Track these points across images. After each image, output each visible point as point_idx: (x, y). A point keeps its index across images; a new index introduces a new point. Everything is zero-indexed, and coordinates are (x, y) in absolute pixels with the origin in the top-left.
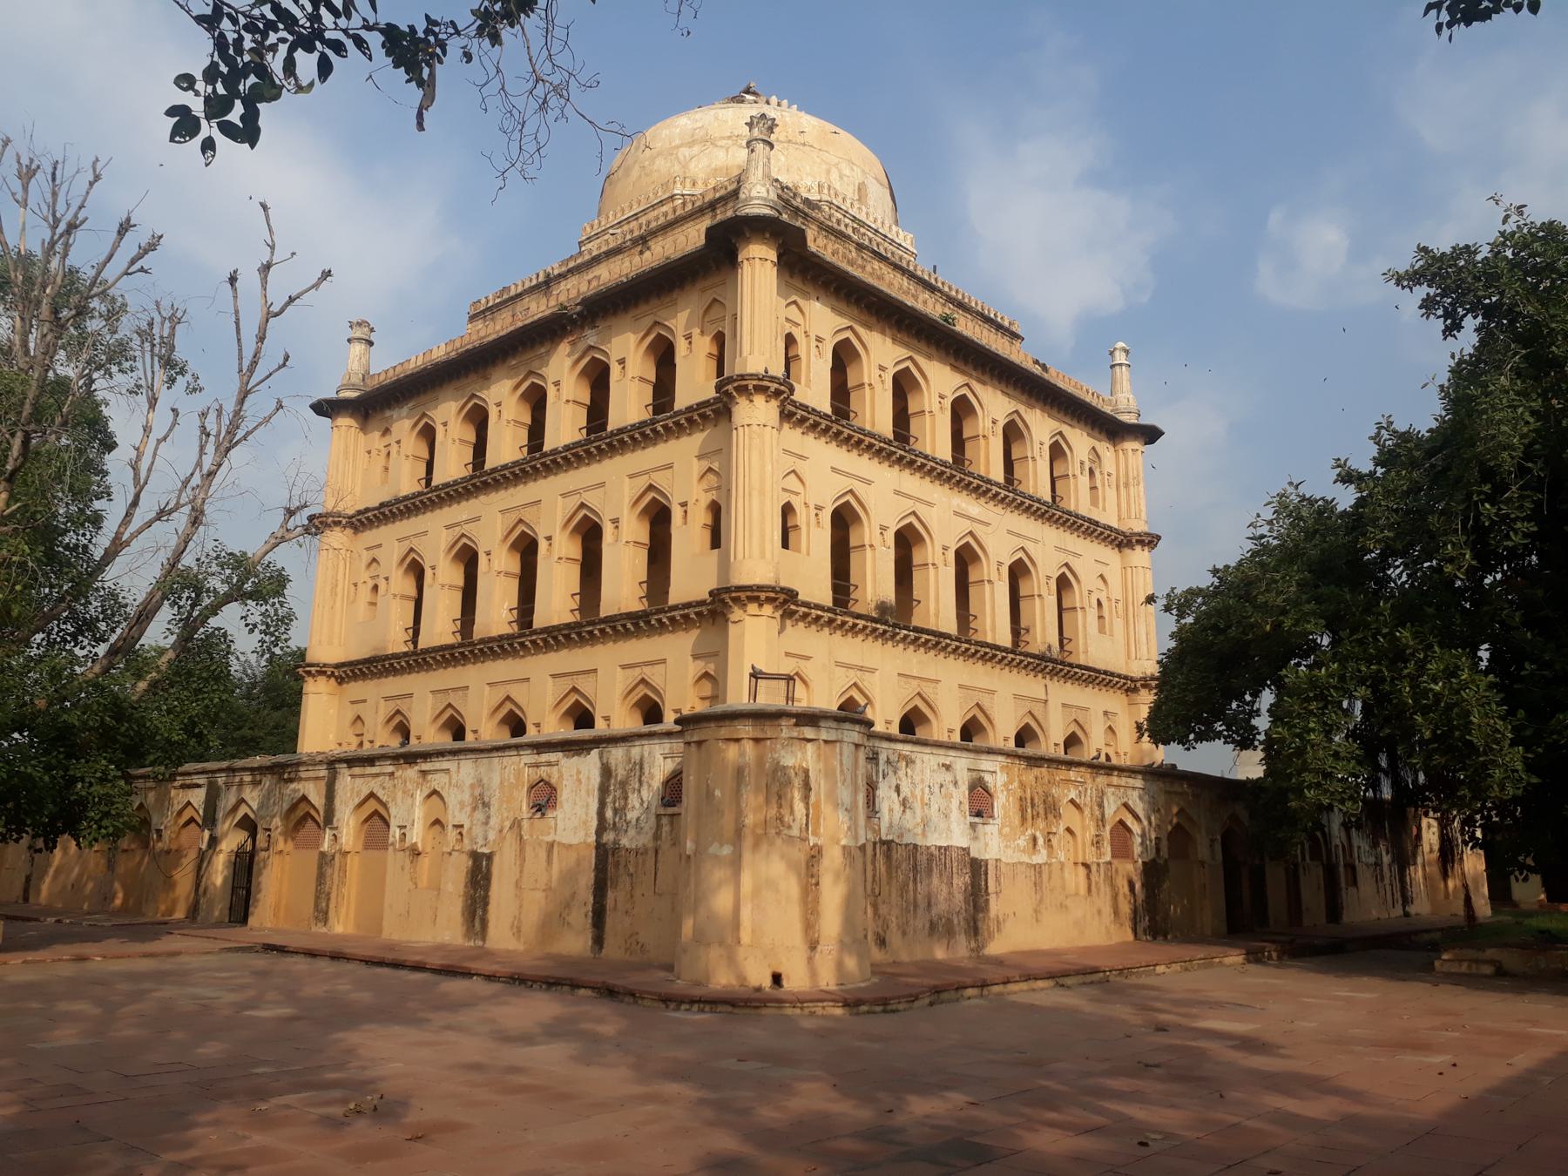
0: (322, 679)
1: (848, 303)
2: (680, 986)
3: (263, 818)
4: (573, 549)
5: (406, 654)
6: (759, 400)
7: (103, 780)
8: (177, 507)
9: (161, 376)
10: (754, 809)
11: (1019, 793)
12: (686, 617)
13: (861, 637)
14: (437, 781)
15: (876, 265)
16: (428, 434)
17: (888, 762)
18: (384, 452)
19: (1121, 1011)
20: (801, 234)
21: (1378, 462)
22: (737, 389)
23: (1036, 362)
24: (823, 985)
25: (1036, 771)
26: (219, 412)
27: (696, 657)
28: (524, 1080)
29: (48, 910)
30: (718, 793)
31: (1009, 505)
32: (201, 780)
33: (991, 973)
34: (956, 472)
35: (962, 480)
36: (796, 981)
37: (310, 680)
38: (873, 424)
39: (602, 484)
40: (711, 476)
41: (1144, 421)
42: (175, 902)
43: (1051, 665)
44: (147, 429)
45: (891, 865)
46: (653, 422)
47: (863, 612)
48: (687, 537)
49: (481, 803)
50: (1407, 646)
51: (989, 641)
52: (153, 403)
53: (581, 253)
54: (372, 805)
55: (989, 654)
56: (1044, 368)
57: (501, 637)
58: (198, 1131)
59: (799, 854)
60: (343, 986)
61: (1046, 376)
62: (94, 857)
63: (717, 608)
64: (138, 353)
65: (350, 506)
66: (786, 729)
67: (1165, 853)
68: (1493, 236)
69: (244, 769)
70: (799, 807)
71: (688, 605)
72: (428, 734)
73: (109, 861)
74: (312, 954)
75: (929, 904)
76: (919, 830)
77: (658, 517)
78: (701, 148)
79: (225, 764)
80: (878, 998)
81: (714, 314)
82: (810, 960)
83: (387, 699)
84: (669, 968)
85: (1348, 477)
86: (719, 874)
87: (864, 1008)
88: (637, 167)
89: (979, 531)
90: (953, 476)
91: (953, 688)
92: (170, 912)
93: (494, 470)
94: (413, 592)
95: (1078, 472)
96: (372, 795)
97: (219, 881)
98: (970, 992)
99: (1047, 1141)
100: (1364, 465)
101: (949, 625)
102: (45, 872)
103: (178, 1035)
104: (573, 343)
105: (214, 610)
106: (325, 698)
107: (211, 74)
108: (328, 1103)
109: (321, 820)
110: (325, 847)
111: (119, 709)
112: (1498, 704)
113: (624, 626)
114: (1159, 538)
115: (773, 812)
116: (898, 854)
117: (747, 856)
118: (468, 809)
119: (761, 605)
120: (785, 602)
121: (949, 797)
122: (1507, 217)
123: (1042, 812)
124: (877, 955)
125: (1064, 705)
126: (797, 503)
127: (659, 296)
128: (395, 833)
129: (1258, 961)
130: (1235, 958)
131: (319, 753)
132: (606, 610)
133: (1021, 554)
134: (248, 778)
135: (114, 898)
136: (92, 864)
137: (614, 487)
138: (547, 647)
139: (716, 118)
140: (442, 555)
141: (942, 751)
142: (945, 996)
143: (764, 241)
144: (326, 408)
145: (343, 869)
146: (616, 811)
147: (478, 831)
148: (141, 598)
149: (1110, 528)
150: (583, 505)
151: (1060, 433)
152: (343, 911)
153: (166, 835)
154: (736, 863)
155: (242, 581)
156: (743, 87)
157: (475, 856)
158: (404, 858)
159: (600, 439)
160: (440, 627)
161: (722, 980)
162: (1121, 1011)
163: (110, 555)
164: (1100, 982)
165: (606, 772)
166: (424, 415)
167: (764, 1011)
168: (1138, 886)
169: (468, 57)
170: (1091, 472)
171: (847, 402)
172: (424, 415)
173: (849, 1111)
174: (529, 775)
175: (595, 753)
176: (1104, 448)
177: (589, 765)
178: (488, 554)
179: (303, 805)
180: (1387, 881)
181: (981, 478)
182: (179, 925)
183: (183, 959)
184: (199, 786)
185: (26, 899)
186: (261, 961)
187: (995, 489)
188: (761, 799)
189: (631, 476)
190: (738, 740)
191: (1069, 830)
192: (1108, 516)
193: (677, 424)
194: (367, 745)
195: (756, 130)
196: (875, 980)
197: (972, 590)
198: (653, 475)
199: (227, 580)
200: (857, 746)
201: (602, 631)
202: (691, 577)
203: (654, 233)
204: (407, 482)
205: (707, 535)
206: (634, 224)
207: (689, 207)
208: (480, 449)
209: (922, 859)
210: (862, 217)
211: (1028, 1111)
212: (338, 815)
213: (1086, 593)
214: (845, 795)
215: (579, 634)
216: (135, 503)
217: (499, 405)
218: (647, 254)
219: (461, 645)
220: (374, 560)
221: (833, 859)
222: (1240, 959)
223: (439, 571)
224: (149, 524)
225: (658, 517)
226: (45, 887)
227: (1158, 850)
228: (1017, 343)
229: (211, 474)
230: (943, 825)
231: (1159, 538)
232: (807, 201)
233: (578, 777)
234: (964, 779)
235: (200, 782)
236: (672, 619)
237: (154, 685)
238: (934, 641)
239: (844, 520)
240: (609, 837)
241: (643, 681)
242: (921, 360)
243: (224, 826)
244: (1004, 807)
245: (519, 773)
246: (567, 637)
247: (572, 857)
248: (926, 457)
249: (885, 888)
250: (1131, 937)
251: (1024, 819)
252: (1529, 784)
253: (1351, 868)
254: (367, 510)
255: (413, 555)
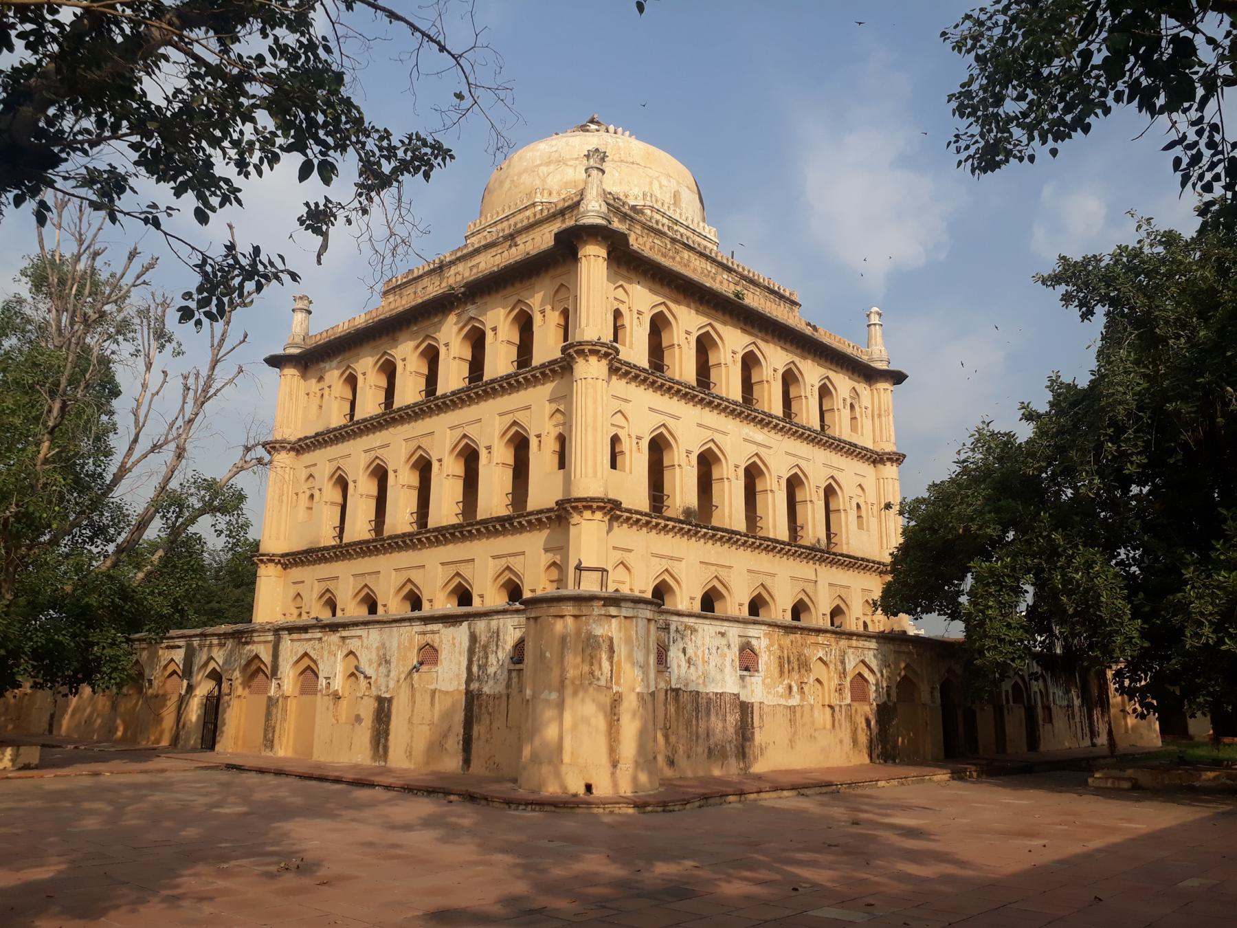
0: (271, 566)
1: (662, 285)
2: (522, 793)
3: (227, 671)
4: (458, 468)
5: (333, 547)
6: (593, 360)
7: (113, 644)
8: (166, 442)
9: (154, 344)
10: (574, 665)
11: (778, 653)
12: (539, 520)
13: (671, 534)
14: (353, 644)
15: (686, 254)
16: (352, 381)
17: (677, 631)
18: (319, 394)
19: (839, 812)
20: (624, 237)
21: (1052, 405)
22: (576, 352)
23: (809, 324)
24: (622, 793)
25: (792, 637)
26: (197, 376)
27: (546, 550)
28: (399, 852)
29: (68, 740)
30: (548, 654)
31: (787, 433)
32: (181, 642)
33: (751, 785)
34: (746, 408)
35: (749, 415)
36: (603, 789)
37: (262, 566)
38: (681, 375)
39: (479, 420)
40: (558, 415)
41: (892, 367)
42: (162, 732)
43: (819, 555)
44: (144, 386)
45: (679, 709)
46: (516, 375)
47: (674, 516)
48: (541, 460)
49: (385, 661)
50: (1059, 546)
51: (771, 536)
52: (149, 366)
53: (466, 246)
54: (306, 662)
55: (771, 546)
56: (815, 328)
57: (404, 535)
58: (185, 879)
59: (606, 700)
60: (283, 793)
61: (816, 335)
62: (102, 702)
63: (561, 515)
64: (138, 327)
65: (292, 432)
66: (597, 609)
67: (894, 698)
68: (1112, 249)
69: (213, 635)
70: (606, 665)
71: (541, 512)
72: (352, 609)
73: (113, 702)
74: (261, 771)
75: (708, 735)
76: (701, 681)
77: (520, 445)
78: (553, 168)
79: (198, 631)
80: (665, 802)
81: (562, 295)
82: (613, 774)
83: (319, 580)
84: (515, 781)
85: (1030, 416)
86: (549, 713)
87: (649, 809)
88: (508, 181)
89: (763, 452)
90: (742, 412)
91: (742, 572)
92: (158, 741)
93: (400, 409)
94: (340, 500)
95: (841, 407)
96: (306, 654)
97: (194, 718)
98: (731, 798)
99: (733, 888)
100: (1043, 408)
101: (739, 524)
102: (65, 711)
103: (167, 824)
104: (459, 315)
105: (193, 520)
106: (274, 579)
107: (200, 290)
108: (268, 864)
109: (268, 673)
110: (272, 693)
111: (125, 593)
112: (1121, 589)
113: (494, 527)
114: (904, 456)
115: (586, 668)
116: (684, 698)
117: (568, 701)
118: (375, 665)
119: (593, 512)
120: (612, 509)
121: (724, 656)
122: (1140, 227)
123: (796, 667)
124: (668, 773)
125: (830, 585)
126: (623, 435)
127: (521, 281)
128: (322, 682)
129: (961, 779)
130: (942, 776)
131: (268, 623)
132: (481, 515)
133: (796, 470)
134: (215, 642)
135: (116, 729)
136: (100, 706)
137: (488, 423)
138: (438, 542)
139: (567, 144)
140: (361, 473)
141: (718, 623)
142: (711, 801)
143: (597, 243)
144: (276, 361)
145: (285, 710)
146: (479, 667)
147: (382, 681)
148: (140, 510)
149: (866, 449)
150: (465, 436)
151: (827, 377)
152: (284, 740)
153: (155, 683)
154: (561, 706)
155: (212, 499)
156: (589, 118)
157: (380, 700)
158: (328, 701)
159: (477, 387)
160: (360, 527)
161: (552, 789)
162: (839, 812)
163: (117, 479)
164: (832, 793)
165: (473, 638)
166: (349, 367)
167: (578, 811)
168: (873, 723)
169: (349, 222)
170: (852, 406)
171: (661, 358)
172: (349, 367)
173: (614, 871)
174: (419, 640)
175: (465, 624)
176: (863, 388)
177: (461, 633)
178: (395, 471)
179: (256, 661)
180: (1077, 719)
181: (764, 413)
182: (165, 750)
183: (168, 774)
184: (179, 647)
185: (51, 732)
186: (224, 776)
187: (775, 421)
188: (579, 659)
189: (501, 415)
190: (562, 617)
191: (818, 680)
192: (865, 440)
193: (534, 376)
194: (304, 616)
195: (592, 161)
196: (662, 789)
197: (759, 498)
198: (517, 414)
199: (202, 499)
200: (649, 620)
201: (478, 530)
202: (544, 490)
203: (520, 232)
204: (336, 417)
205: (556, 458)
206: (505, 224)
207: (545, 213)
208: (390, 392)
209: (702, 702)
210: (677, 217)
211: (731, 871)
212: (281, 669)
213: (847, 499)
214: (639, 656)
215: (461, 533)
216: (135, 441)
217: (404, 360)
218: (514, 249)
219: (374, 541)
220: (311, 475)
221: (630, 702)
222: (947, 777)
223: (359, 484)
224: (145, 456)
225: (520, 445)
226: (65, 722)
227: (889, 695)
228: (796, 309)
229: (191, 421)
230: (719, 677)
231: (904, 456)
232: (633, 208)
233: (453, 641)
234: (736, 643)
235: (181, 644)
236: (529, 522)
237: (149, 574)
238: (729, 537)
239: (658, 447)
240: (474, 686)
241: (508, 568)
242: (718, 326)
243: (198, 677)
244: (766, 664)
245: (411, 639)
246: (453, 535)
247: (448, 702)
248: (721, 398)
249: (674, 724)
250: (867, 761)
251: (782, 672)
252: (1142, 647)
253: (1047, 709)
254: (306, 438)
255: (340, 472)
